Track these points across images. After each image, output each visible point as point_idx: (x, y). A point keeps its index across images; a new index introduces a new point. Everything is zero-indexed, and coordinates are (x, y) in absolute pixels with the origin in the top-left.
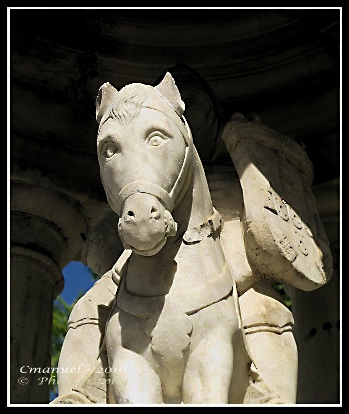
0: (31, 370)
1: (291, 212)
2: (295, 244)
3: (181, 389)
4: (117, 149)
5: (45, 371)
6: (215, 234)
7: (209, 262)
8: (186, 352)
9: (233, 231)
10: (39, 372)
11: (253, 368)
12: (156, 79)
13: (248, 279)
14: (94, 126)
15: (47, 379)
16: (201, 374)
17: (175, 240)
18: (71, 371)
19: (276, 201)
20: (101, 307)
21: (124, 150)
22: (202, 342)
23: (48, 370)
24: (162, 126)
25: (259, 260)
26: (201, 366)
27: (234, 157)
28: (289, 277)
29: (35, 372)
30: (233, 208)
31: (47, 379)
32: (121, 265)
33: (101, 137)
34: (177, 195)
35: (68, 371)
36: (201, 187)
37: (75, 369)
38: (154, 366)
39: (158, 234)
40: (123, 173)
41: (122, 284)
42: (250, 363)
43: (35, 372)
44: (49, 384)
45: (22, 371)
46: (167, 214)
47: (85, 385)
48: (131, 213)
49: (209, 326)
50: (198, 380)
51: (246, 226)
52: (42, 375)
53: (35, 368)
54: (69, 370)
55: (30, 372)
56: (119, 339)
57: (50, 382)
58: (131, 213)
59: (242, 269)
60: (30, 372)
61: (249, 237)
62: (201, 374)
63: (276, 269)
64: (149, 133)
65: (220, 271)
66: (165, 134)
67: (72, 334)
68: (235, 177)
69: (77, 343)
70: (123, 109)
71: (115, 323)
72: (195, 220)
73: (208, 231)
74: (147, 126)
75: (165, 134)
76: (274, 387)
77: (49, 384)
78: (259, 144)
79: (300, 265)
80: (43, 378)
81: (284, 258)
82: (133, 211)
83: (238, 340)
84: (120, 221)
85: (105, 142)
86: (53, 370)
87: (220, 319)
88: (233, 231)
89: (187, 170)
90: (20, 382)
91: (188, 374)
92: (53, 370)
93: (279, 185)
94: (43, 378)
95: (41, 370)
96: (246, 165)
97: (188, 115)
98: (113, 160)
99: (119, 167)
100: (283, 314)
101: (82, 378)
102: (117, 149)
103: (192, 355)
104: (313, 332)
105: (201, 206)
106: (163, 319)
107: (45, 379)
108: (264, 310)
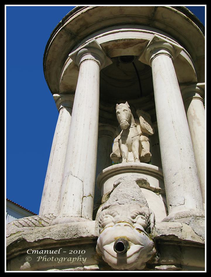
0: (33, 252)
1: (147, 123)
2: (148, 128)
3: (131, 149)
4: (119, 113)
6: (136, 126)
7: (135, 130)
8: (132, 144)
9: (138, 127)
10: (37, 253)
12: (53, 43)
13: (141, 134)
14: (115, 110)
15: (42, 257)
16: (134, 147)
17: (129, 127)
19: (145, 122)
20: (118, 139)
21: (120, 113)
22: (134, 142)
23: (42, 252)
24: (126, 109)
25: (143, 131)
26: (134, 145)
27: (138, 115)
28: (147, 133)
29: (35, 253)
30: (138, 123)
33: (117, 112)
34: (129, 120)
36: (133, 119)
39: (126, 125)
40: (120, 117)
41: (122, 136)
42: (142, 146)
43: (35, 253)
44: (43, 261)
45: (28, 252)
46: (127, 122)
47: (116, 151)
48: (122, 123)
49: (135, 140)
50: (134, 148)
51: (140, 125)
52: (39, 255)
55: (33, 253)
56: (121, 143)
57: (43, 259)
58: (122, 123)
59: (140, 132)
60: (33, 253)
61: (141, 127)
62: (134, 147)
63: (145, 132)
64: (124, 110)
65: (136, 131)
66: (127, 110)
67: (114, 143)
68: (138, 118)
69: (115, 145)
70: (120, 107)
71: (121, 141)
72: (132, 124)
73: (134, 126)
74: (124, 109)
75: (127, 110)
76: (163, 228)
78: (195, 138)
79: (149, 131)
80: (40, 257)
81: (147, 130)
83: (140, 142)
84: (120, 124)
85: (117, 112)
86: (45, 252)
87: (137, 138)
88: (138, 127)
90: (27, 259)
91: (132, 147)
92: (45, 252)
93: (145, 119)
96: (140, 116)
97: (130, 108)
98: (119, 115)
99: (120, 116)
100: (147, 139)
101: (116, 150)
102: (119, 113)
103: (133, 144)
104: (153, 145)
105: (133, 122)
106: (128, 139)
107: (40, 258)
108: (144, 138)
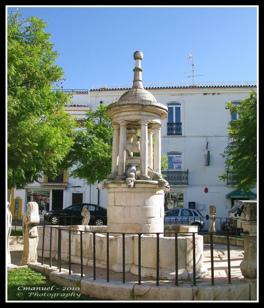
5: (32, 289)
11: (86, 295)
18: (76, 289)
29: (26, 290)
31: (51, 294)
32: (96, 248)
35: (36, 289)
37: (50, 288)
38: (97, 181)
43: (26, 290)
44: (35, 296)
52: (30, 291)
53: (27, 288)
54: (46, 289)
55: (24, 290)
57: (35, 295)
60: (24, 290)
77: (35, 296)
82: (206, 193)
89: (79, 247)
94: (31, 293)
95: (30, 289)
107: (32, 294)
